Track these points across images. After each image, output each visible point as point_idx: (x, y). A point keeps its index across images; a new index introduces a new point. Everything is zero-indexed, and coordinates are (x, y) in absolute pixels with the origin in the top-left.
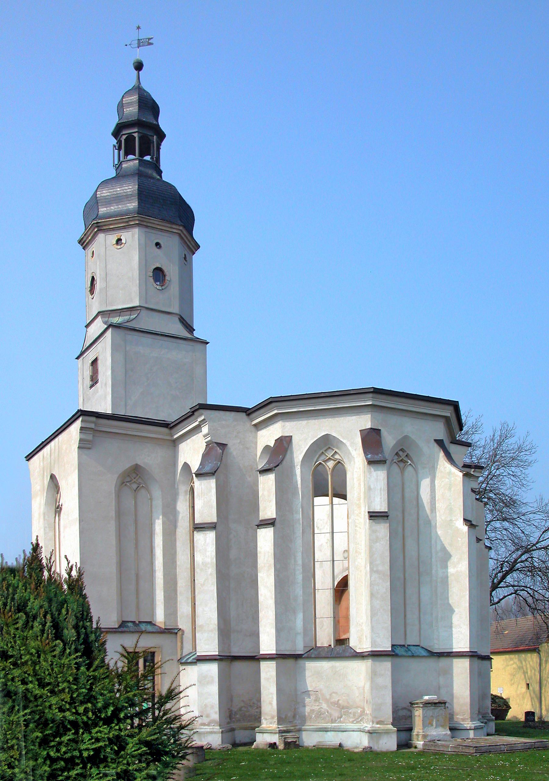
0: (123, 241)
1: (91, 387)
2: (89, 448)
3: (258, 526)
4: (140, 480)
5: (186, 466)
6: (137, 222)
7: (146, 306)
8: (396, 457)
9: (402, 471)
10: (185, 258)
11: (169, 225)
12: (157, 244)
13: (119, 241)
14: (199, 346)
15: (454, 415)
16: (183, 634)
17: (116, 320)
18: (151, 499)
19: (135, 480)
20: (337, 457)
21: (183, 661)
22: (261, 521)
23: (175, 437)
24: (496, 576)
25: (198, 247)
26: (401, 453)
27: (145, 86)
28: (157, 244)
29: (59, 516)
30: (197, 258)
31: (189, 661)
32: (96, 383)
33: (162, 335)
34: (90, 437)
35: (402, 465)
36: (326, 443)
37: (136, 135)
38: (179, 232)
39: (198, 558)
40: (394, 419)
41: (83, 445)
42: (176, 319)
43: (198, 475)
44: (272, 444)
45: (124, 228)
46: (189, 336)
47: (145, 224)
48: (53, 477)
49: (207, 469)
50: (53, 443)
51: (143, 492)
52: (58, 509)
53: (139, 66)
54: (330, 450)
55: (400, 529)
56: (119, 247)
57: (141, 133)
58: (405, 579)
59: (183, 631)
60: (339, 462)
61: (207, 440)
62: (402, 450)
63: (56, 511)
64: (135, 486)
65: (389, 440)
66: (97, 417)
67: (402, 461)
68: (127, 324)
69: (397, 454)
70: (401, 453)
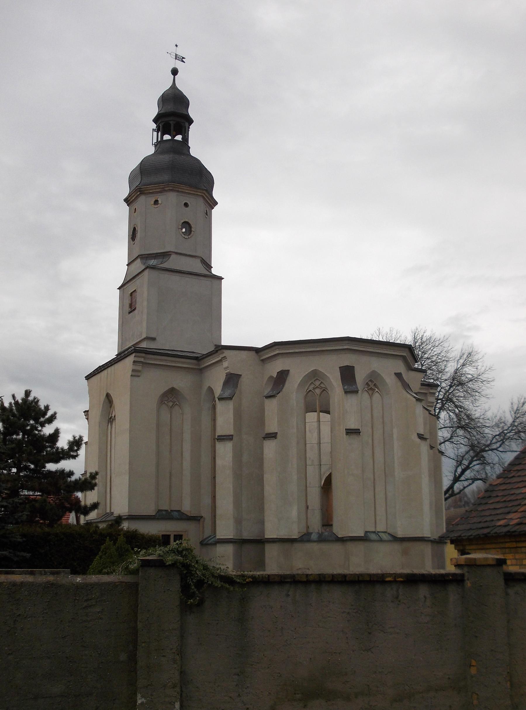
0: (160, 202)
1: (130, 313)
2: (139, 376)
3: (264, 438)
4: (175, 400)
5: (211, 390)
6: (171, 188)
7: (176, 251)
8: (367, 386)
9: (371, 396)
10: (206, 214)
11: (195, 190)
12: (186, 205)
13: (156, 202)
14: (216, 282)
15: (409, 354)
16: (204, 521)
17: (152, 262)
18: (183, 414)
19: (171, 399)
20: (322, 385)
21: (205, 542)
22: (266, 434)
23: (203, 366)
24: (456, 471)
25: (216, 203)
26: (370, 383)
27: (180, 86)
28: (186, 205)
29: (111, 425)
30: (215, 211)
31: (210, 542)
32: (134, 310)
33: (187, 273)
34: (139, 368)
35: (370, 392)
36: (315, 375)
37: (171, 122)
38: (203, 195)
39: (219, 462)
40: (364, 359)
41: (135, 374)
43: (220, 399)
44: (275, 375)
45: (161, 192)
46: (208, 273)
47: (177, 189)
48: (108, 396)
49: (227, 394)
50: (109, 369)
51: (177, 408)
52: (111, 420)
53: (175, 72)
54: (317, 381)
55: (370, 441)
56: (156, 206)
57: (174, 115)
58: (374, 479)
59: (204, 518)
60: (324, 390)
61: (226, 371)
62: (371, 381)
63: (109, 421)
64: (171, 404)
65: (360, 377)
66: (145, 353)
68: (161, 266)
69: (367, 384)
70: (370, 383)
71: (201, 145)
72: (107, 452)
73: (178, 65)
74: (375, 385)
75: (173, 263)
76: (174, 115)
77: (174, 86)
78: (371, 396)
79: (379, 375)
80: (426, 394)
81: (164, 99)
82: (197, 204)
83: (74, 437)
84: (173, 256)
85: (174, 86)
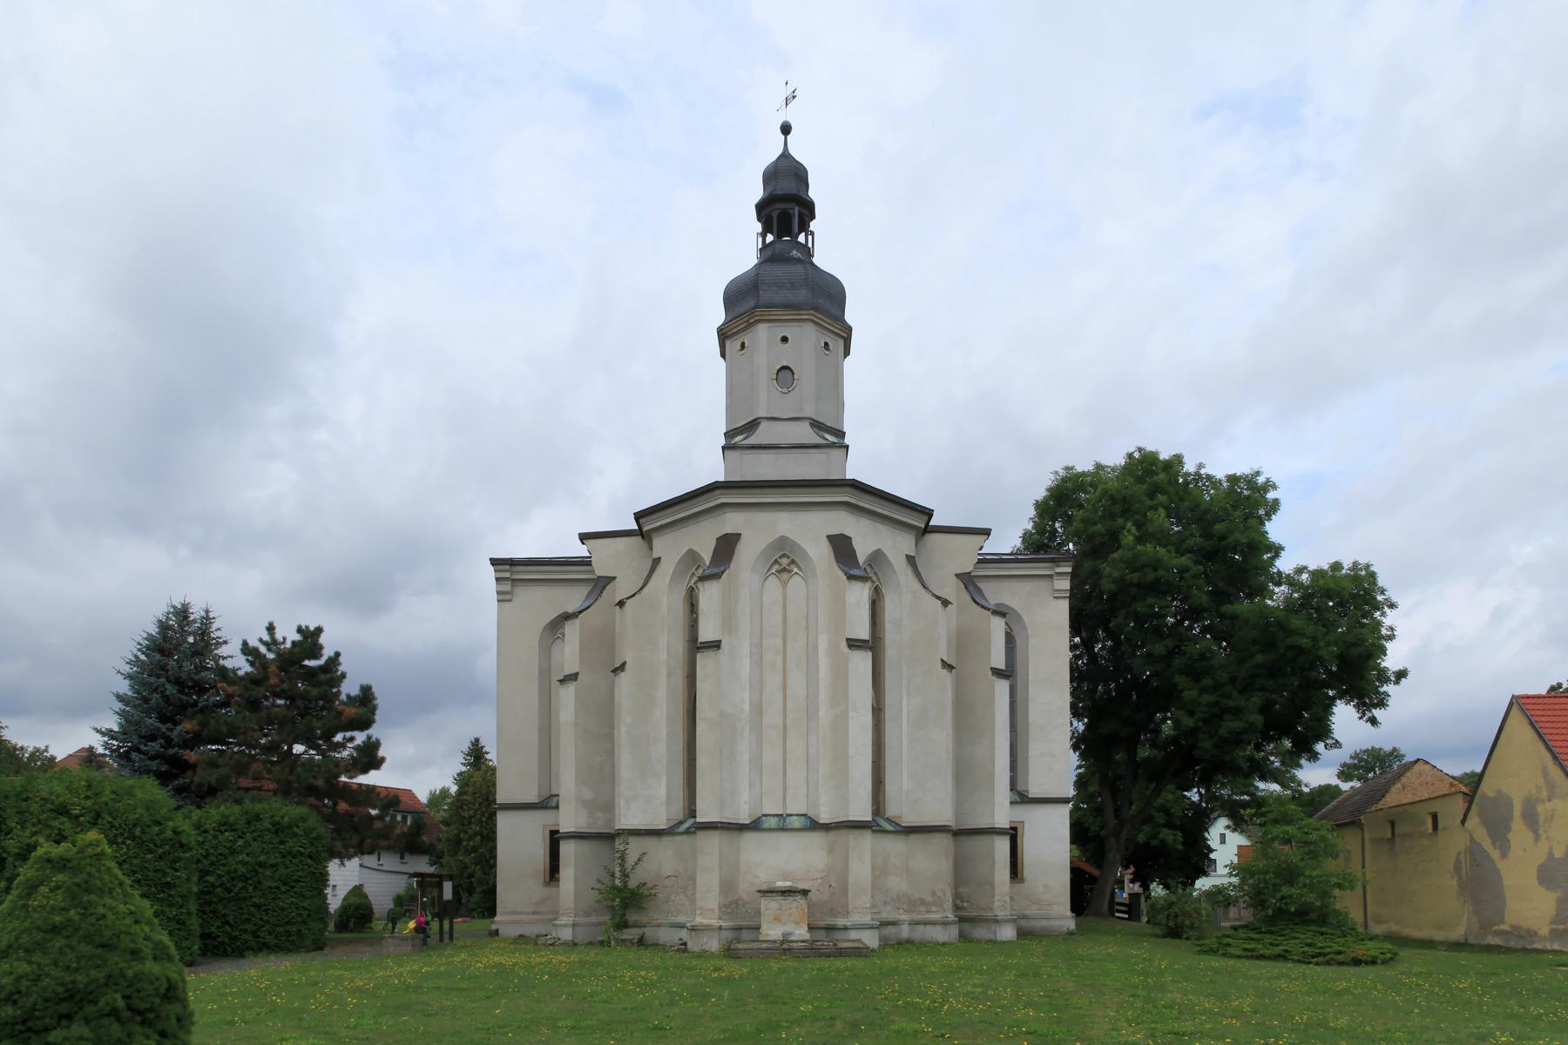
9: (785, 584)
12: (785, 339)
13: (743, 346)
34: (507, 587)
35: (785, 576)
42: (807, 424)
53: (786, 129)
57: (786, 205)
67: (784, 570)
71: (831, 245)
72: (840, 725)
73: (790, 115)
74: (793, 562)
75: (761, 435)
76: (786, 205)
77: (785, 155)
78: (785, 584)
79: (794, 543)
80: (1051, 576)
81: (771, 176)
82: (807, 336)
83: (120, 698)
84: (764, 425)
85: (785, 155)
